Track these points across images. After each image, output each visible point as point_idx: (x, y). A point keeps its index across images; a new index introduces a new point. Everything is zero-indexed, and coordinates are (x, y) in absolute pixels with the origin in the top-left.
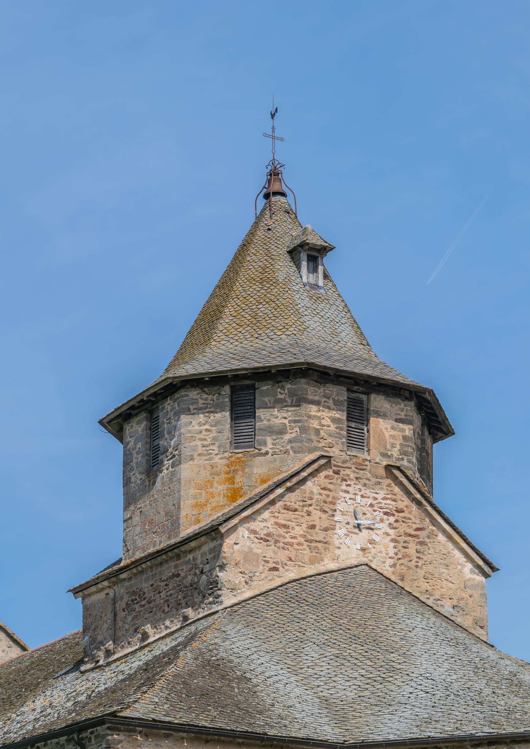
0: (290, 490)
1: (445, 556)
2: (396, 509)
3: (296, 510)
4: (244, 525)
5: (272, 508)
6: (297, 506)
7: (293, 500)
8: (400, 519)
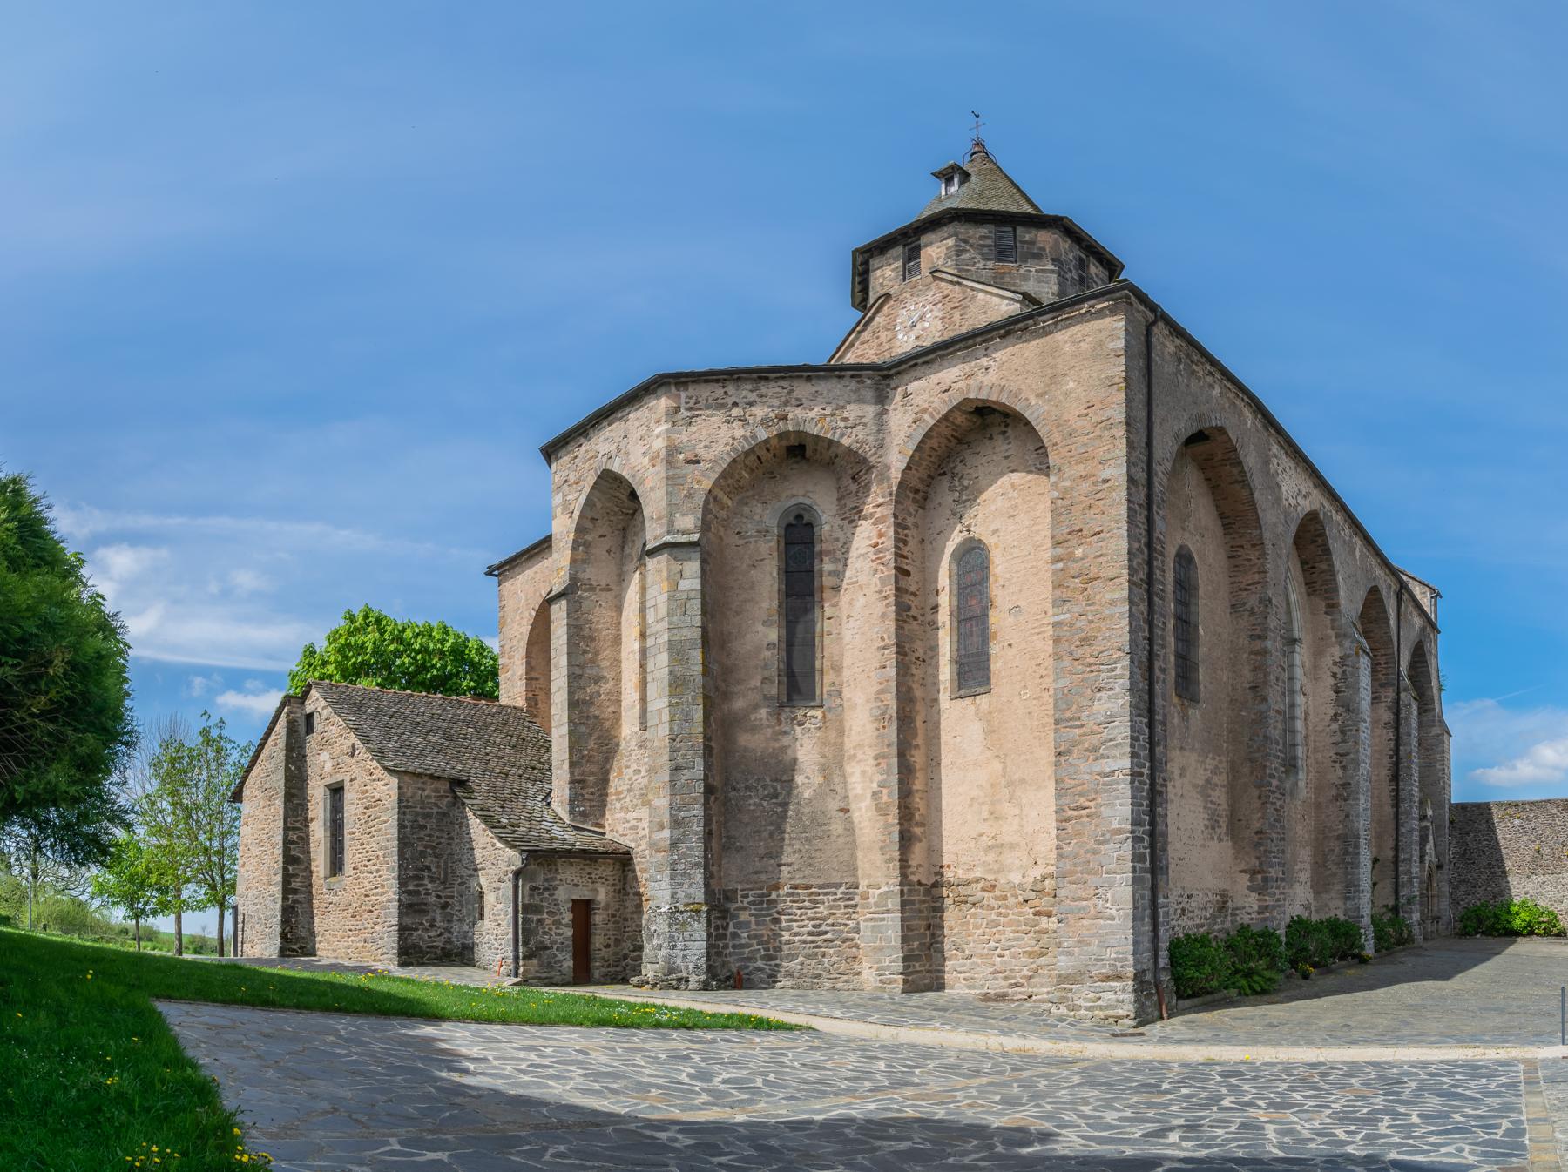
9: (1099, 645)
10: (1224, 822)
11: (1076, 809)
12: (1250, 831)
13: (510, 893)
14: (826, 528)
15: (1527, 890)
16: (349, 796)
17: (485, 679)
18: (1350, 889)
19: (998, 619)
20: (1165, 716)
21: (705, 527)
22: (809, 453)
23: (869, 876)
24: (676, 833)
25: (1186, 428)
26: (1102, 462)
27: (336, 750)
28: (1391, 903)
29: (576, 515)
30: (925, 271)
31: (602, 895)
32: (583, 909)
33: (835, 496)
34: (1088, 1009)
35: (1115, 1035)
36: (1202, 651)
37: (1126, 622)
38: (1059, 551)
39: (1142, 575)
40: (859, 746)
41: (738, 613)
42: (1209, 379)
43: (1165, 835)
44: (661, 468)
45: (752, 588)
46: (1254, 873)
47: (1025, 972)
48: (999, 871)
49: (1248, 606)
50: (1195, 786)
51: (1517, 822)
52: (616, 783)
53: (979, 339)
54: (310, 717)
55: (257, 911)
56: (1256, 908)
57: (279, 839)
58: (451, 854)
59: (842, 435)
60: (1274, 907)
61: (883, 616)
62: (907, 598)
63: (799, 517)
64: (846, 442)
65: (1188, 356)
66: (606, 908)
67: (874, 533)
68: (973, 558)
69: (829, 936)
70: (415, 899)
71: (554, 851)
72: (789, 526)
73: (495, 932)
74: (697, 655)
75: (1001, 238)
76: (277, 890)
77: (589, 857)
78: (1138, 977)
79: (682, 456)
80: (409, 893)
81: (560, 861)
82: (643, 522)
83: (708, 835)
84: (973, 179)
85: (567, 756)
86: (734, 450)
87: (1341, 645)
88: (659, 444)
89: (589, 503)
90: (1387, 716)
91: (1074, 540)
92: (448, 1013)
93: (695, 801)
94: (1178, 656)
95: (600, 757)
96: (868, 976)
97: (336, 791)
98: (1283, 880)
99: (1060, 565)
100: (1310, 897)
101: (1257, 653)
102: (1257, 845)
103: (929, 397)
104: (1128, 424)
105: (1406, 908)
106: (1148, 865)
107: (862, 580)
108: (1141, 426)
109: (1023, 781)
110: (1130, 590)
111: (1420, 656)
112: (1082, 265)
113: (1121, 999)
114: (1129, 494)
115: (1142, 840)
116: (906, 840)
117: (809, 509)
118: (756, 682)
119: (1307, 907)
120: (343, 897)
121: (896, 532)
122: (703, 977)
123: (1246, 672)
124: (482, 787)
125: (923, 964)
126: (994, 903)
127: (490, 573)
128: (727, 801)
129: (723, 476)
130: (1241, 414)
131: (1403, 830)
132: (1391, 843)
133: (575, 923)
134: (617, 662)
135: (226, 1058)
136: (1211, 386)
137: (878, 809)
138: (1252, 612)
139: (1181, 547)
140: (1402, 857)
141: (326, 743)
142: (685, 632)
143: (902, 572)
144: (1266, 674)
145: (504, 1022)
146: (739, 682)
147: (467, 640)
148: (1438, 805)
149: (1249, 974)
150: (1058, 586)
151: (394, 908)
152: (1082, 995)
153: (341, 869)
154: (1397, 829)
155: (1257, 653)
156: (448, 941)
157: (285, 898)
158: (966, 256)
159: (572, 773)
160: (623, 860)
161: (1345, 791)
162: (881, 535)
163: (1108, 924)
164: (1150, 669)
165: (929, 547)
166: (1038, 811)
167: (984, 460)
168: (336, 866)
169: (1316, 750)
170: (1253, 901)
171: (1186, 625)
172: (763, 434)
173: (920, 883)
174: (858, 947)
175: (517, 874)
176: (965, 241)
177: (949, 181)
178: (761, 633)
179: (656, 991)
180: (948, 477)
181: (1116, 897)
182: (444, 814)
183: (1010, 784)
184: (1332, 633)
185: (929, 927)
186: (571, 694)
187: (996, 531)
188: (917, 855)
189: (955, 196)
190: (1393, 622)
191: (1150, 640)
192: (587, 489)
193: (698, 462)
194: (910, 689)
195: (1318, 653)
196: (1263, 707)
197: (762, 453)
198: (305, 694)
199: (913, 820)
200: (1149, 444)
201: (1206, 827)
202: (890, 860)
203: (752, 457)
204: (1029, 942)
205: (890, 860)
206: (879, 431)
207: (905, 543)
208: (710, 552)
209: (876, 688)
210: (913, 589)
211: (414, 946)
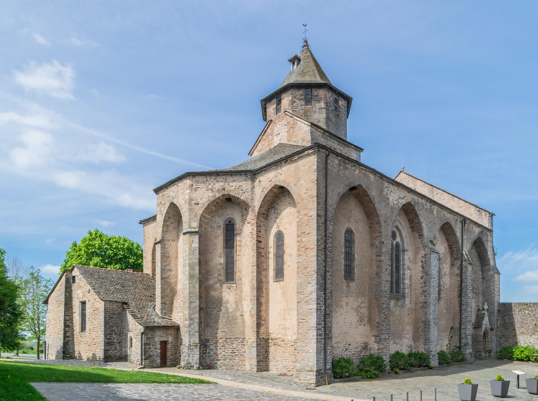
9: (309, 270)
10: (366, 320)
11: (302, 319)
12: (377, 320)
13: (140, 339)
14: (238, 226)
15: (526, 340)
16: (88, 306)
17: (138, 267)
18: (427, 341)
19: (286, 257)
20: (332, 290)
21: (200, 226)
22: (232, 200)
23: (248, 336)
24: (191, 322)
25: (342, 189)
26: (310, 210)
27: (83, 290)
28: (458, 345)
29: (164, 215)
30: (283, 111)
31: (170, 339)
32: (164, 344)
33: (241, 214)
34: (304, 380)
35: (307, 389)
36: (356, 263)
37: (316, 263)
38: (299, 239)
39: (322, 246)
40: (246, 296)
41: (211, 253)
42: (354, 168)
43: (331, 328)
44: (187, 205)
45: (215, 245)
46: (376, 336)
47: (292, 367)
48: (285, 336)
49: (376, 245)
50: (353, 308)
51: (527, 312)
52: (176, 304)
54: (74, 277)
55: (54, 343)
56: (377, 348)
57: (62, 319)
58: (122, 326)
59: (241, 196)
60: (383, 348)
61: (253, 256)
62: (260, 250)
63: (230, 222)
64: (242, 198)
65: (344, 162)
66: (172, 343)
67: (251, 229)
68: (280, 236)
69: (236, 354)
70: (110, 341)
71: (154, 326)
72: (227, 225)
73: (135, 351)
74: (197, 268)
75: (307, 95)
76: (62, 337)
77: (166, 328)
78: (317, 371)
79: (193, 202)
80: (108, 339)
81: (156, 330)
82: (182, 223)
83: (200, 323)
84: (302, 62)
85: (160, 295)
86: (209, 200)
87: (424, 250)
88: (187, 197)
89: (167, 212)
90: (457, 272)
91: (303, 235)
92: (118, 380)
93: (196, 312)
94: (346, 265)
95: (171, 296)
96: (248, 367)
97: (83, 303)
98: (389, 339)
99: (299, 244)
100: (412, 343)
101: (378, 261)
102: (377, 327)
103: (267, 181)
104: (317, 196)
105: (464, 347)
106: (323, 337)
107: (248, 243)
108: (323, 196)
109: (292, 309)
110: (317, 252)
111: (479, 245)
112: (336, 101)
113: (312, 378)
114: (317, 221)
115: (321, 329)
116: (259, 325)
117: (233, 219)
118: (216, 275)
119: (411, 347)
120: (85, 339)
121: (257, 229)
122: (198, 366)
123: (375, 268)
124: (133, 304)
125: (263, 362)
126: (284, 346)
127: (140, 223)
128: (207, 313)
129: (206, 209)
130: (368, 176)
131: (463, 316)
132: (458, 321)
133: (161, 348)
134: (176, 265)
135: (51, 396)
136: (355, 171)
137: (251, 316)
138: (377, 247)
139: (348, 228)
140: (463, 327)
141: (80, 287)
142: (194, 260)
143: (259, 242)
144: (381, 269)
145: (126, 383)
146: (211, 275)
147: (133, 243)
148: (491, 303)
149: (367, 371)
150: (298, 250)
151: (102, 344)
152: (302, 376)
153: (85, 330)
154: (461, 316)
155: (378, 261)
156: (121, 354)
157: (64, 339)
158: (295, 104)
159: (162, 300)
160: (177, 328)
161: (425, 305)
162: (253, 229)
163: (310, 357)
164: (325, 276)
165: (268, 233)
166: (292, 319)
167: (283, 204)
168: (83, 329)
169: (415, 289)
170: (376, 346)
171: (349, 256)
172: (218, 195)
173: (263, 338)
174: (245, 357)
175: (142, 334)
176: (295, 97)
177: (294, 63)
178: (218, 260)
179: (184, 370)
180: (273, 209)
181: (311, 347)
182: (120, 313)
183: (288, 309)
184: (421, 245)
185: (266, 352)
186: (162, 275)
187: (286, 229)
188: (263, 330)
189: (294, 75)
190: (458, 234)
191: (325, 267)
192: (167, 208)
193: (198, 204)
194: (261, 279)
195: (416, 253)
196: (380, 280)
197: (218, 201)
198: (73, 269)
199: (261, 320)
200: (326, 201)
201: (358, 321)
202: (254, 331)
203: (215, 203)
204: (293, 358)
205: (254, 331)
206: (252, 194)
207: (260, 232)
208: (203, 235)
209: (251, 278)
210: (263, 247)
211: (109, 356)
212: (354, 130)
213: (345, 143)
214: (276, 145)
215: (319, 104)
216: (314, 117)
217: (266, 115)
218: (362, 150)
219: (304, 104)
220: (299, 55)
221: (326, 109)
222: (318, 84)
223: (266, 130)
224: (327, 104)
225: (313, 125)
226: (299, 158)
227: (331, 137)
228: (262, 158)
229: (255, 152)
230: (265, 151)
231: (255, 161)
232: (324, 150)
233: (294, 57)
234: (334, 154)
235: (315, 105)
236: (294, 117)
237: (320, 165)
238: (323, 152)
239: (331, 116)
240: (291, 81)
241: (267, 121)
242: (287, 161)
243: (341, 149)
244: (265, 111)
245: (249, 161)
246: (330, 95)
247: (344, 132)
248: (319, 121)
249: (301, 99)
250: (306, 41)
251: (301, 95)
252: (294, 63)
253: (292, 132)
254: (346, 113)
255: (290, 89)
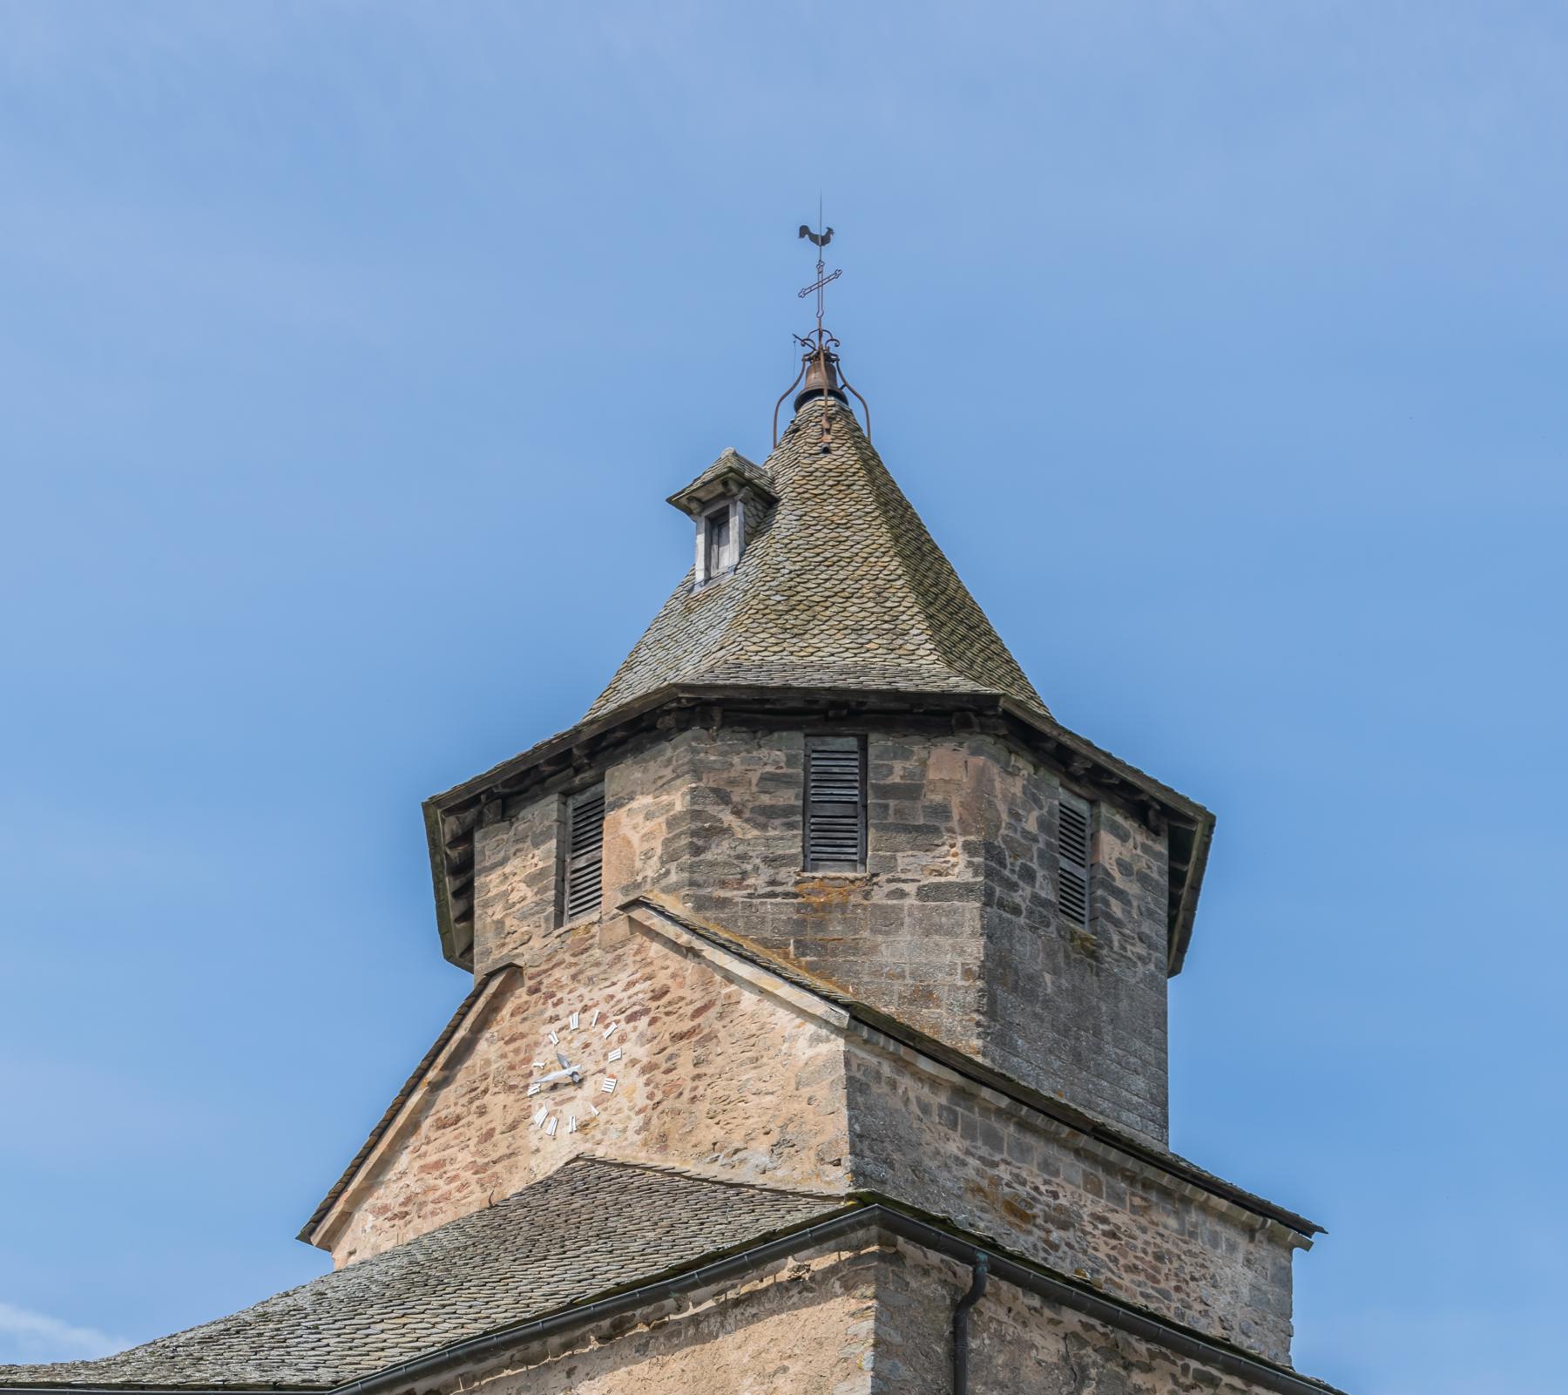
0: (436, 1087)
1: (753, 1040)
2: (650, 995)
3: (458, 1119)
4: (365, 1206)
5: (414, 1142)
6: (459, 1110)
7: (452, 1100)
8: (660, 1013)
30: (612, 897)
53: (555, 1341)
65: (1111, 1351)
75: (826, 778)
84: (784, 520)
112: (1073, 836)
158: (719, 851)
176: (722, 797)
177: (716, 526)
212: (1231, 1060)
213: (1151, 1173)
214: (547, 1164)
215: (925, 859)
216: (886, 956)
217: (468, 915)
218: (1306, 1229)
219: (796, 849)
220: (763, 457)
221: (989, 899)
222: (921, 696)
223: (468, 1046)
224: (991, 855)
225: (864, 1022)
226: (723, 1310)
227: (1023, 1126)
228: (421, 1275)
229: (364, 1219)
230: (448, 1216)
231: (357, 1302)
232: (934, 1257)
233: (723, 479)
234: (1029, 1287)
235: (889, 864)
236: (710, 953)
237: (905, 1372)
238: (930, 1279)
239: (1030, 952)
240: (690, 669)
241: (482, 967)
242: (619, 1328)
243: (1121, 1219)
244: (466, 891)
245: (305, 1300)
246: (1017, 787)
247: (1140, 1083)
248: (925, 995)
249: (769, 813)
250: (825, 359)
251: (772, 781)
252: (716, 526)
253: (685, 1069)
254: (1157, 931)
255: (683, 727)
